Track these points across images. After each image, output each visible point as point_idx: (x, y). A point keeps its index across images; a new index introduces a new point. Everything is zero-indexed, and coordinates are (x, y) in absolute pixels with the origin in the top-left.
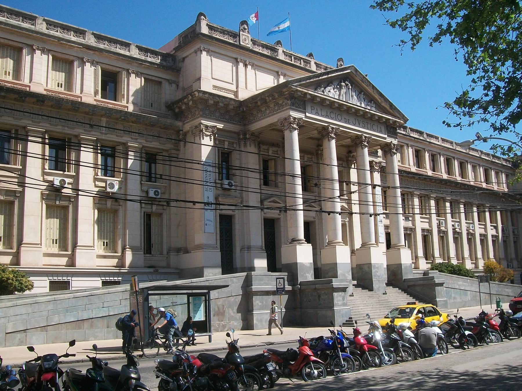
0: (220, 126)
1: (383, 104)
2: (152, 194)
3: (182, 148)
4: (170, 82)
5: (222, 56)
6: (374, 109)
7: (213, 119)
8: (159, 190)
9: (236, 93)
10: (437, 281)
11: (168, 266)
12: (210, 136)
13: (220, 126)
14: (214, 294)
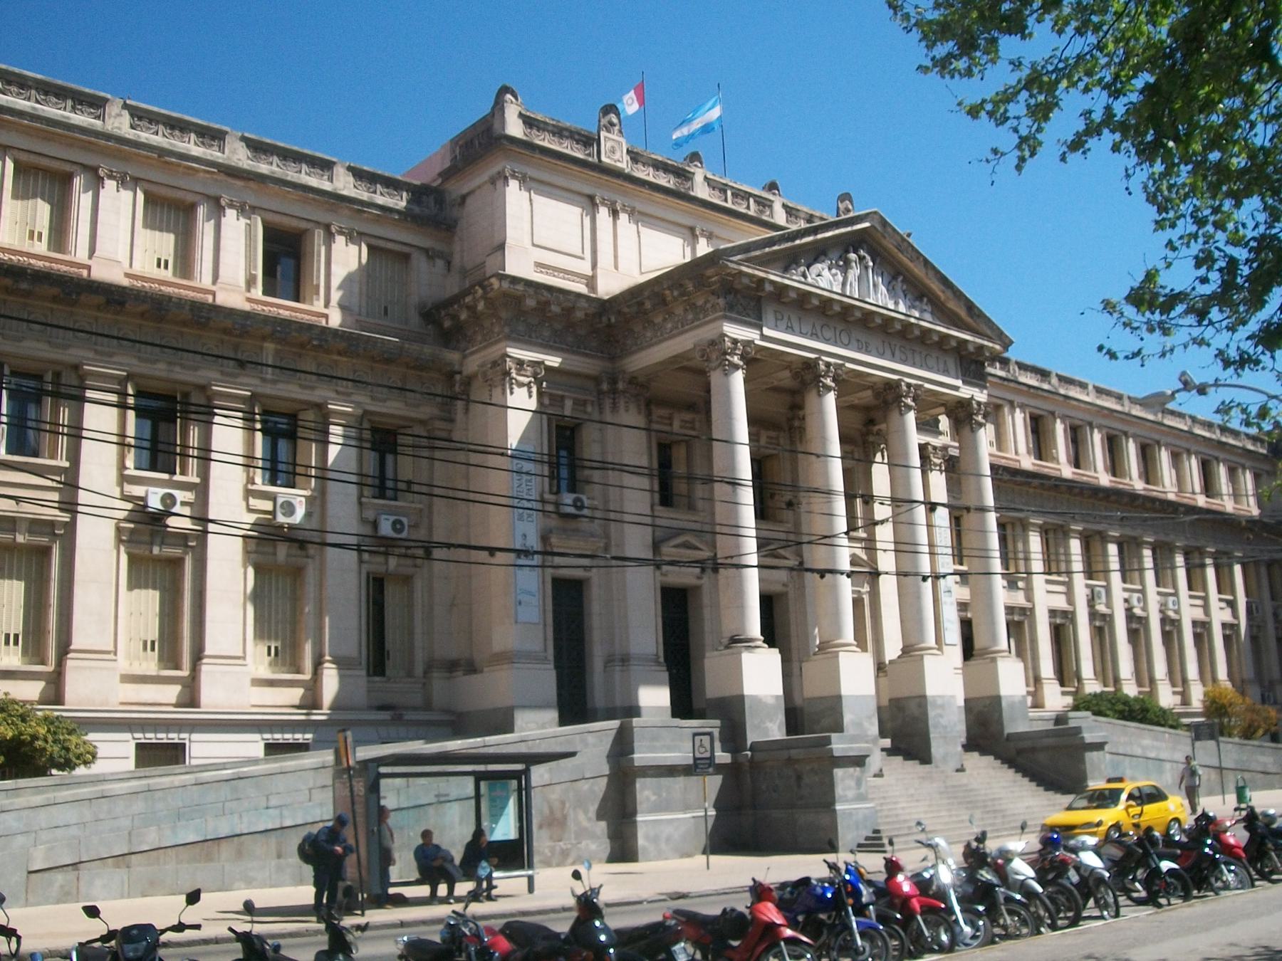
0: (554, 361)
1: (952, 305)
2: (386, 529)
3: (460, 416)
4: (430, 255)
5: (547, 189)
6: (928, 316)
7: (535, 344)
8: (405, 520)
9: (591, 281)
10: (1089, 737)
11: (428, 706)
12: (529, 385)
13: (554, 361)
14: (539, 774)
